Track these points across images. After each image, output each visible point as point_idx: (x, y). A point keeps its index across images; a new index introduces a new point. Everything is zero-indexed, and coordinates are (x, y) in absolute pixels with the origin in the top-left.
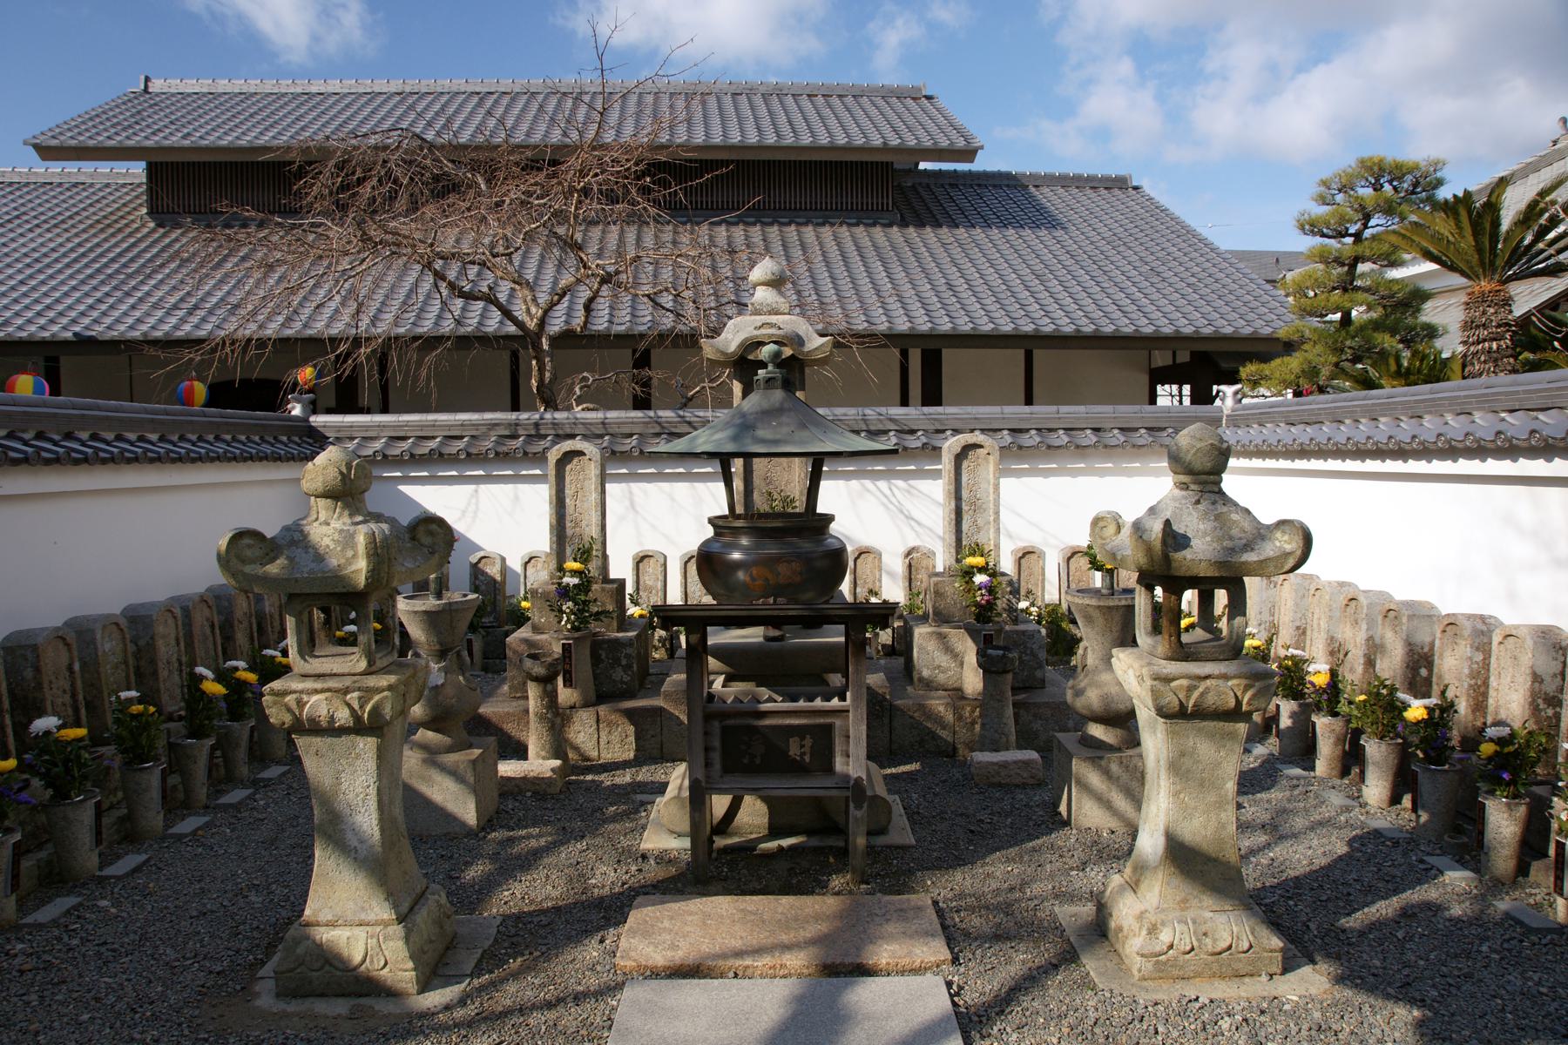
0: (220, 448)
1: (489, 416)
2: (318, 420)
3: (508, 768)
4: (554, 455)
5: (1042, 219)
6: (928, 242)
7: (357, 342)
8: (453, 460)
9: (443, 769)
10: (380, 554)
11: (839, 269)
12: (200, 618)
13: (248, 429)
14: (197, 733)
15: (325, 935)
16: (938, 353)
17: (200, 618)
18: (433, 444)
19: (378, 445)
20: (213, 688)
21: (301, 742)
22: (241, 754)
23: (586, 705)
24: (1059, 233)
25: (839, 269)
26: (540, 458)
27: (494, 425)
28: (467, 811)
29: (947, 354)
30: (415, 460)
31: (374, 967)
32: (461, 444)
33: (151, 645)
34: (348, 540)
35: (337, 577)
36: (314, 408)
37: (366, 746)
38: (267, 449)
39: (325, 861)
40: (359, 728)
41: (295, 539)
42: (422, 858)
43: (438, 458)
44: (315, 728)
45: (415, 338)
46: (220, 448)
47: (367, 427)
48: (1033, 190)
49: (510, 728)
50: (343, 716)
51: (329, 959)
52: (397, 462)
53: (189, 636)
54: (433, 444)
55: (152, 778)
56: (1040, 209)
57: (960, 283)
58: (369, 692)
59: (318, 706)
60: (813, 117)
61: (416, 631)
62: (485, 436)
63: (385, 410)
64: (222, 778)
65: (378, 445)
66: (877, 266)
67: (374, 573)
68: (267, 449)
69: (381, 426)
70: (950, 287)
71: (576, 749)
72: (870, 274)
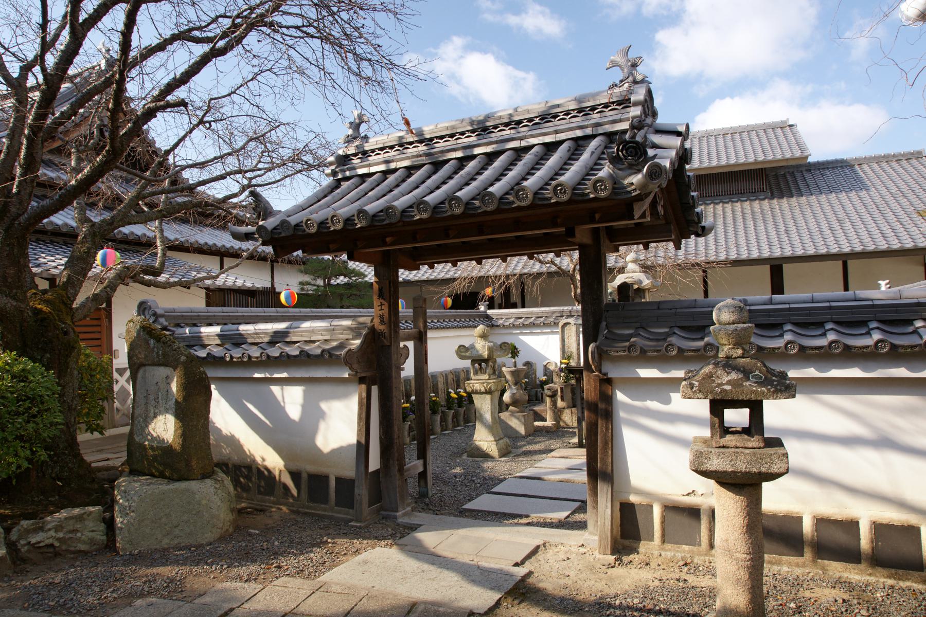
0: (456, 324)
1: (552, 308)
2: (490, 312)
3: (537, 423)
4: (560, 325)
5: (858, 184)
6: (784, 206)
7: (508, 277)
8: (538, 326)
9: (516, 417)
10: (490, 350)
11: (730, 228)
12: (450, 377)
13: (465, 317)
14: (449, 409)
15: (477, 443)
16: (781, 266)
17: (450, 377)
18: (531, 320)
19: (511, 321)
20: (453, 395)
21: (474, 396)
22: (461, 418)
23: (568, 408)
24: (863, 193)
25: (730, 228)
26: (556, 324)
27: (554, 312)
28: (522, 430)
29: (786, 267)
30: (524, 326)
31: (488, 451)
32: (541, 320)
33: (437, 384)
34: (484, 346)
35: (481, 356)
36: (491, 307)
37: (488, 397)
38: (471, 323)
39: (479, 426)
40: (486, 392)
41: (472, 347)
42: (503, 432)
43: (533, 325)
44: (477, 393)
45: (530, 275)
46: (456, 324)
47: (507, 314)
48: (857, 167)
49: (543, 414)
50: (483, 389)
51: (478, 449)
52: (518, 327)
53: (447, 383)
54: (531, 320)
55: (438, 418)
56: (858, 179)
57: (792, 229)
58: (489, 383)
59: (478, 387)
60: (722, 148)
61: (509, 377)
62: (551, 316)
63: (523, 307)
64: (456, 423)
65: (511, 321)
66: (750, 224)
67: (489, 355)
68: (471, 323)
69: (513, 314)
70: (787, 231)
71: (565, 422)
72: (745, 228)
